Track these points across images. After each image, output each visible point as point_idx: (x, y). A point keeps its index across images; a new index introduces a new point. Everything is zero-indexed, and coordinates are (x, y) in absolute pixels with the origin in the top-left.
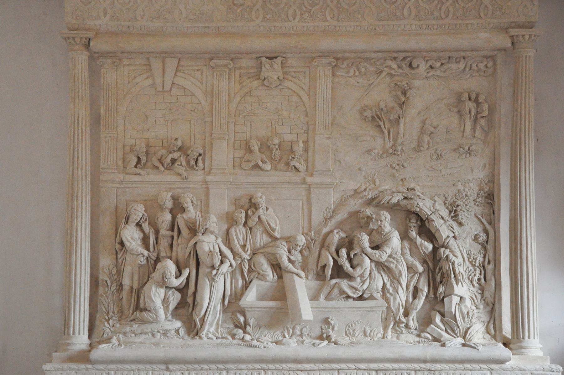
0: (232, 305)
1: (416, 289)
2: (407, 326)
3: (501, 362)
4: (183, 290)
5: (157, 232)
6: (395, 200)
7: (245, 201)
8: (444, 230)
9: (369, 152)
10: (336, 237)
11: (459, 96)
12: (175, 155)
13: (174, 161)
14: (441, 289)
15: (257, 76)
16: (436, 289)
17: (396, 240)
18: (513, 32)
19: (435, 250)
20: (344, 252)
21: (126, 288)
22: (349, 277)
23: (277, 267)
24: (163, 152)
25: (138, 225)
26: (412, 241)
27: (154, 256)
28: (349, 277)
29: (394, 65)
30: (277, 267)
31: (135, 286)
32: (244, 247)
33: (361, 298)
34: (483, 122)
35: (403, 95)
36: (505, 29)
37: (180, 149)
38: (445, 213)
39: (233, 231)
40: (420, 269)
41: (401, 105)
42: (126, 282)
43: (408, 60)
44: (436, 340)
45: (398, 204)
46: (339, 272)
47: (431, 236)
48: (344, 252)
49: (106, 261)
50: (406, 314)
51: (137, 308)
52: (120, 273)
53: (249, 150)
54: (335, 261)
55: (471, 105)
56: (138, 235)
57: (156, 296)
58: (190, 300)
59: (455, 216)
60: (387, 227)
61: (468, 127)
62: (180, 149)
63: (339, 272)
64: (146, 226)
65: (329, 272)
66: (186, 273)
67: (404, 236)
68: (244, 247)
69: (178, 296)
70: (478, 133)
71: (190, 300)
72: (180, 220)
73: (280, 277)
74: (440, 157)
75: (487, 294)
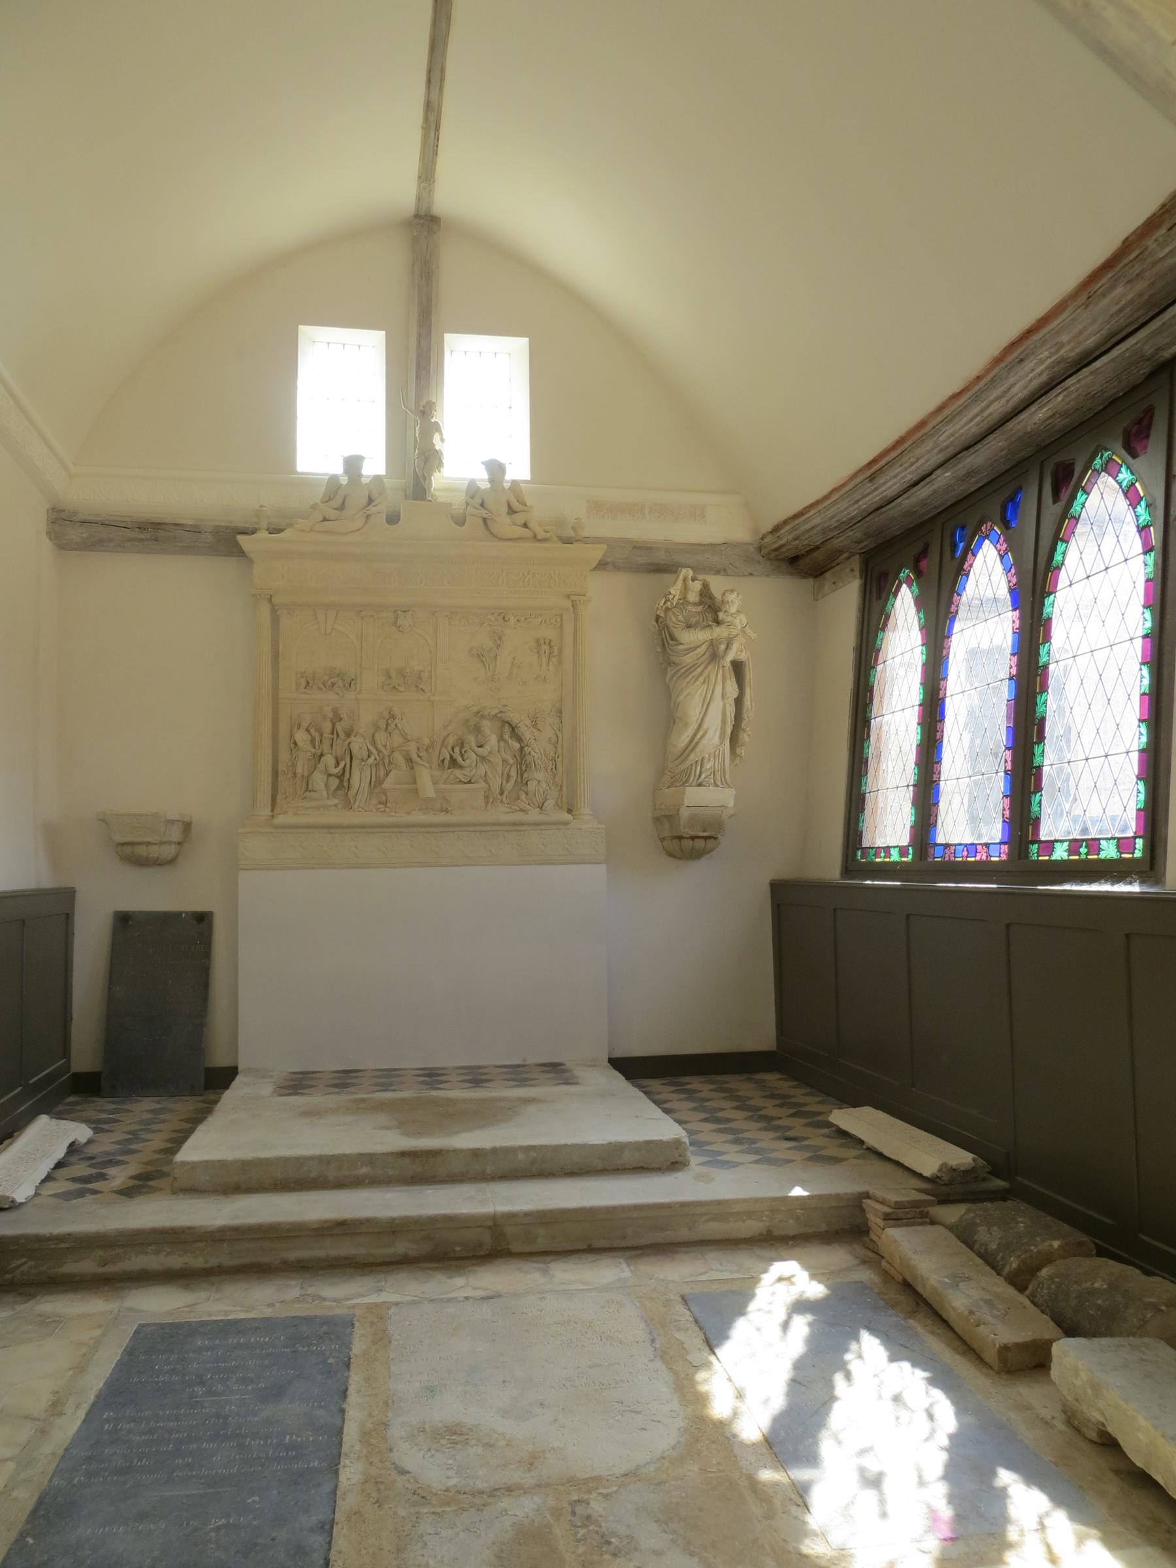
0: (376, 784)
1: (509, 776)
2: (502, 801)
3: (567, 824)
4: (341, 777)
5: (321, 735)
6: (493, 713)
7: (386, 714)
8: (527, 733)
9: (475, 679)
10: (451, 740)
11: (538, 641)
12: (334, 680)
13: (333, 685)
14: (525, 775)
15: (395, 624)
16: (522, 775)
17: (493, 740)
18: (573, 598)
19: (522, 748)
20: (457, 750)
21: (299, 776)
22: (461, 767)
23: (409, 760)
24: (326, 678)
25: (307, 730)
26: (506, 742)
27: (319, 753)
28: (461, 767)
29: (492, 618)
30: (409, 760)
31: (306, 774)
32: (385, 746)
33: (470, 782)
34: (554, 659)
35: (498, 640)
36: (568, 596)
37: (338, 676)
38: (528, 722)
39: (377, 735)
40: (511, 761)
41: (498, 646)
42: (299, 770)
43: (503, 615)
44: (522, 810)
45: (496, 715)
46: (453, 763)
47: (519, 739)
48: (457, 750)
49: (284, 756)
50: (502, 793)
51: (307, 790)
52: (294, 765)
53: (390, 677)
54: (451, 756)
55: (546, 647)
56: (307, 737)
57: (318, 779)
58: (346, 784)
59: (535, 725)
60: (488, 732)
61: (544, 660)
62: (338, 676)
63: (453, 763)
64: (312, 731)
65: (447, 762)
66: (342, 764)
67: (501, 738)
68: (385, 746)
69: (337, 781)
70: (551, 667)
71: (346, 784)
72: (339, 727)
73: (412, 768)
74: (525, 683)
75: (557, 779)
